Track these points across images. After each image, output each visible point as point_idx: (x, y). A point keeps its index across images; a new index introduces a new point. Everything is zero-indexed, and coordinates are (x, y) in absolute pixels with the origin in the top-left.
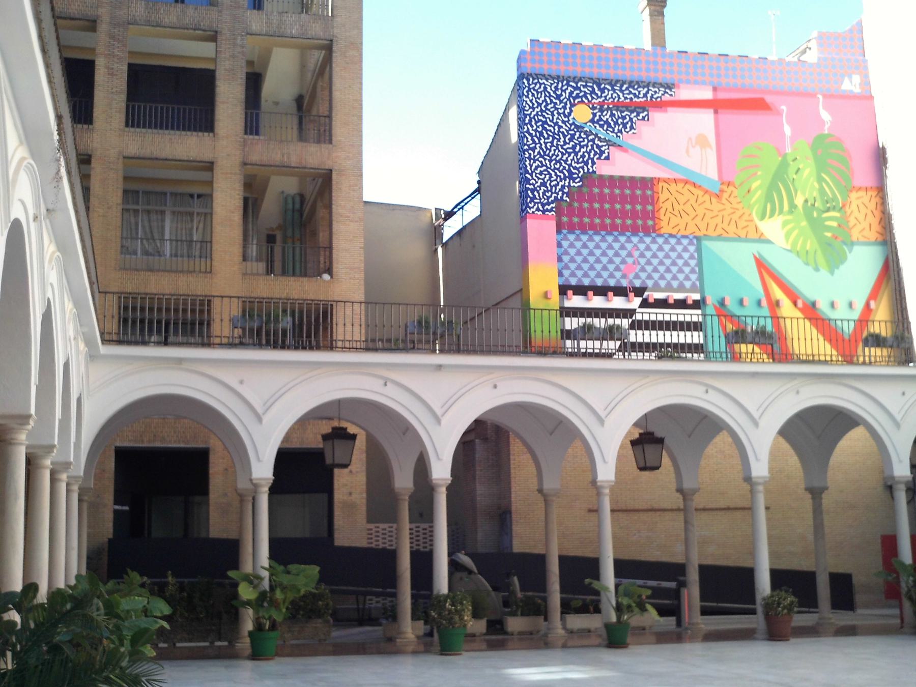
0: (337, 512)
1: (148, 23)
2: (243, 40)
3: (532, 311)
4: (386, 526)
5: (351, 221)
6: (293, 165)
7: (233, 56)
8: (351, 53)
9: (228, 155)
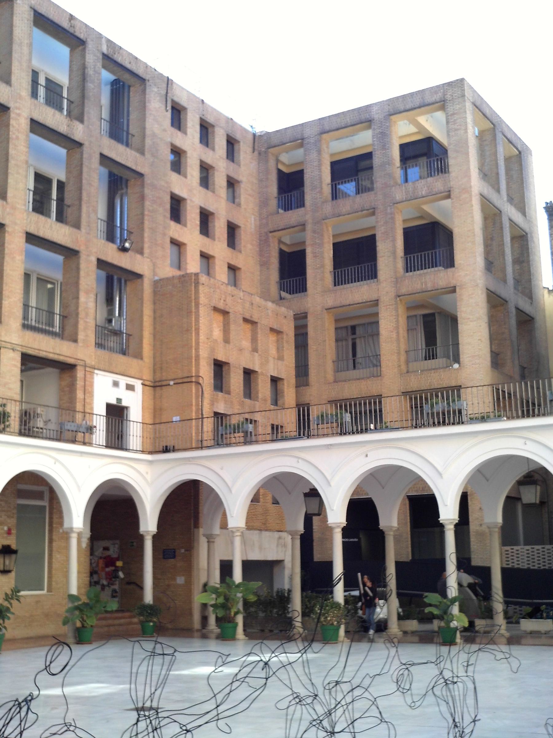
0: (473, 539)
2: (391, 209)
5: (471, 321)
6: (429, 289)
8: (464, 196)
9: (387, 293)
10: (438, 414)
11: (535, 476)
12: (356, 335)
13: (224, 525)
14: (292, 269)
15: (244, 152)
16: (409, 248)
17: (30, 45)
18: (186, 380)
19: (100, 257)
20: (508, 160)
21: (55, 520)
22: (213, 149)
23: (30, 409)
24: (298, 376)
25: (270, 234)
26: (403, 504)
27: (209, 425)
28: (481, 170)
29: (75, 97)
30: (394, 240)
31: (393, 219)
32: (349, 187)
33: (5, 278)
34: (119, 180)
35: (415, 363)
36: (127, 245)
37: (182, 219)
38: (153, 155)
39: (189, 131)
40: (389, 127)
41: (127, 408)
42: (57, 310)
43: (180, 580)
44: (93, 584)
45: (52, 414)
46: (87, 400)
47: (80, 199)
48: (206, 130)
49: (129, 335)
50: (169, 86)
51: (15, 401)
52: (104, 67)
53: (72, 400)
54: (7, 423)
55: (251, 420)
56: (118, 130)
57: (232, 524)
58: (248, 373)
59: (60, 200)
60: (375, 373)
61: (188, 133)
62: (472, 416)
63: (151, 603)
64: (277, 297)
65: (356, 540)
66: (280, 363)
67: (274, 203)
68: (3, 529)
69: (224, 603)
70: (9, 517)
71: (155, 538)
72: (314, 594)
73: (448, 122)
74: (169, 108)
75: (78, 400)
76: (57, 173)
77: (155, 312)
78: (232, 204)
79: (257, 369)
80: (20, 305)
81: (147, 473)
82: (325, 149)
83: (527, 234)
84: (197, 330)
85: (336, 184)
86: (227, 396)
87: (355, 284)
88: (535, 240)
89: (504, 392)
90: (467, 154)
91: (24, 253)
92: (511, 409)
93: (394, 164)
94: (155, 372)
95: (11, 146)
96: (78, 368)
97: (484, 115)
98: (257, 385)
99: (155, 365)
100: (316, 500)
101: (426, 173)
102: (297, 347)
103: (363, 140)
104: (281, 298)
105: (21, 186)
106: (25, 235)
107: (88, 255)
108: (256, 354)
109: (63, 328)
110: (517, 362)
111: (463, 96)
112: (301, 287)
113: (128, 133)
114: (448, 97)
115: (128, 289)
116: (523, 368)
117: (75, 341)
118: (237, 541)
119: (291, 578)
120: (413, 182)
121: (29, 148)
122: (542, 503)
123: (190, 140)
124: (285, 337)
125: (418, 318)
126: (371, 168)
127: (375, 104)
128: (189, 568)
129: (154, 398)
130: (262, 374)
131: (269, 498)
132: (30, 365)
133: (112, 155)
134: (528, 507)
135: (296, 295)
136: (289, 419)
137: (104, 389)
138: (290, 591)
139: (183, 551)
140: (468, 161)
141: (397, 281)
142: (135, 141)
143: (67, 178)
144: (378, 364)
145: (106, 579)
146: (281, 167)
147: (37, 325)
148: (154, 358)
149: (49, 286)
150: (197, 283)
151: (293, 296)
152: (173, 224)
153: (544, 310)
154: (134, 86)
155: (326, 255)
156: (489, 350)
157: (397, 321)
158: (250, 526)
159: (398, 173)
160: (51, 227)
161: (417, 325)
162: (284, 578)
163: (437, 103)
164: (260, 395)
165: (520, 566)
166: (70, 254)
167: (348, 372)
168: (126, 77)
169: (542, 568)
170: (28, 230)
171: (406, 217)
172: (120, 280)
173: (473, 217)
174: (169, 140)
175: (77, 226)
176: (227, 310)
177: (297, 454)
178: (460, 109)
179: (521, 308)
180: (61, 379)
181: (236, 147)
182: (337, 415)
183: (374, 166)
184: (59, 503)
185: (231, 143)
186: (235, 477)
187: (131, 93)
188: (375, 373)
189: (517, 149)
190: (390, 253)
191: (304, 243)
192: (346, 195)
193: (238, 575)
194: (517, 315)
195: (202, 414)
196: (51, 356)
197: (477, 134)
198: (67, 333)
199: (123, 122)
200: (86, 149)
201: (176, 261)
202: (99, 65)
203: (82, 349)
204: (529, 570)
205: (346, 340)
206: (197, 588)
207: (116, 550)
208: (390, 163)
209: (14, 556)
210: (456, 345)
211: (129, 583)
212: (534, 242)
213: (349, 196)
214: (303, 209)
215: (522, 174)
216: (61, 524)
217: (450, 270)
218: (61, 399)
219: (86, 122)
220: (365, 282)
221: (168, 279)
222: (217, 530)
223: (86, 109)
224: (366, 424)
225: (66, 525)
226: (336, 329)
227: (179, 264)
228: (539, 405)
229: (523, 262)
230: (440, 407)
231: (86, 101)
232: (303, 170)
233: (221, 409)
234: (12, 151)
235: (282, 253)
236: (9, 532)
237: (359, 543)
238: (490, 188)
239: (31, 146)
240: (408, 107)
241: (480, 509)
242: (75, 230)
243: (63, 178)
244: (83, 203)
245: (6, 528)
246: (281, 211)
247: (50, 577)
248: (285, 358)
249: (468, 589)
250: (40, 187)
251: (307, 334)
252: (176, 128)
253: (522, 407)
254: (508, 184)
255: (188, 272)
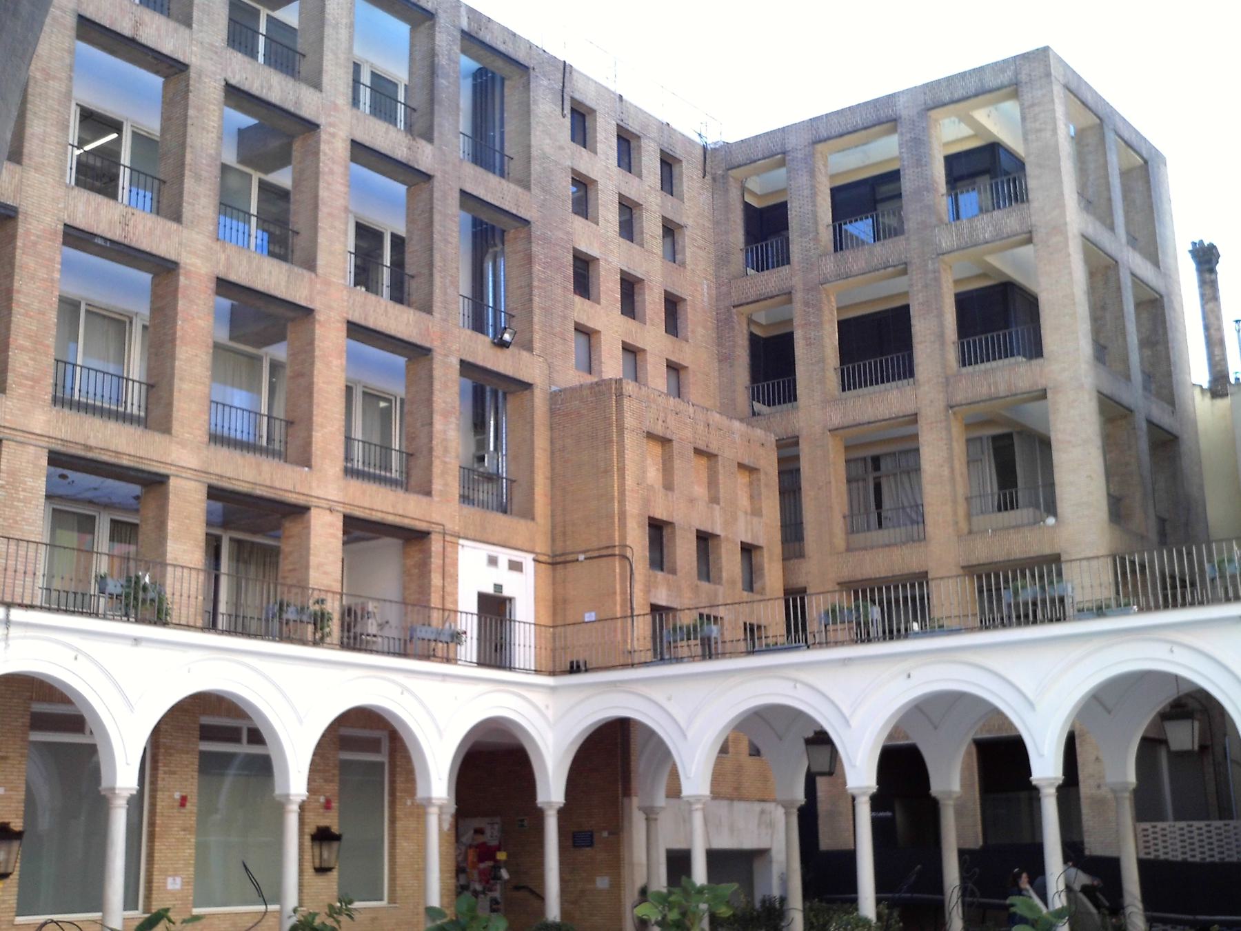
0: (1086, 810)
1: (839, 277)
3: (170, 569)
4: (1202, 824)
7: (926, 286)
10: (1026, 604)
11: (1194, 706)
12: (881, 470)
13: (675, 791)
14: (772, 365)
15: (690, 177)
16: (966, 327)
17: (351, 26)
18: (604, 552)
19: (464, 358)
20: (1125, 174)
21: (400, 785)
22: (640, 176)
23: (356, 604)
24: (785, 541)
25: (734, 310)
26: (968, 753)
27: (642, 627)
28: (1082, 194)
29: (419, 101)
30: (940, 315)
31: (937, 280)
32: (861, 228)
33: (315, 395)
34: (490, 231)
35: (981, 517)
36: (507, 337)
37: (593, 291)
38: (544, 190)
39: (600, 147)
40: (925, 130)
41: (510, 599)
42: (396, 444)
43: (602, 883)
44: (461, 889)
45: (392, 613)
46: (448, 589)
47: (431, 265)
48: (627, 142)
49: (511, 482)
50: (567, 75)
51: (334, 593)
52: (464, 51)
53: (425, 589)
54: (327, 630)
55: (716, 618)
56: (486, 149)
57: (688, 789)
58: (704, 539)
59: (398, 264)
60: (916, 535)
61: (599, 150)
62: (1081, 606)
63: (558, 920)
64: (748, 411)
65: (889, 814)
66: (755, 520)
67: (738, 258)
68: (318, 801)
69: (678, 921)
70: (326, 781)
71: (563, 813)
72: (824, 904)
73: (1024, 119)
74: (567, 111)
75: (433, 589)
76: (392, 223)
77: (552, 443)
78: (671, 264)
79: (718, 531)
80: (341, 438)
81: (547, 707)
82: (822, 167)
83: (1161, 296)
84: (622, 470)
85: (840, 226)
86: (670, 576)
87: (876, 388)
88: (1176, 306)
89: (1133, 563)
90: (1058, 170)
91: (345, 355)
92: (1145, 594)
93: (936, 190)
94: (553, 540)
95: (322, 185)
96: (433, 536)
97: (1083, 103)
98: (719, 558)
99: (553, 527)
100: (824, 751)
101: (990, 203)
102: (782, 492)
103: (882, 151)
104: (754, 414)
105: (338, 247)
106: (345, 326)
107: (446, 356)
108: (717, 507)
109: (407, 473)
110: (1151, 511)
111: (1048, 75)
112: (788, 394)
113: (503, 155)
114: (1023, 77)
115: (508, 406)
116: (1162, 521)
117: (428, 493)
118: (698, 819)
119: (784, 875)
120: (970, 219)
121: (349, 186)
122: (1203, 748)
123: (601, 163)
124: (762, 477)
125: (985, 442)
126: (898, 196)
127: (903, 92)
128: (616, 863)
129: (554, 583)
130: (727, 539)
131: (744, 747)
132: (357, 533)
133: (480, 192)
134: (1178, 757)
135: (778, 407)
136: (773, 616)
137: (475, 569)
138: (783, 900)
139: (605, 834)
140: (1061, 182)
141: (948, 382)
142: (513, 167)
143: (408, 231)
144: (920, 519)
145: (480, 881)
146: (748, 199)
147: (366, 469)
148: (553, 516)
149: (382, 404)
150: (620, 395)
151: (773, 409)
152: (577, 299)
153: (1195, 423)
154: (510, 78)
155: (827, 341)
156: (1105, 493)
157: (950, 449)
158: (716, 795)
159: (943, 203)
160: (386, 311)
161: (983, 452)
162: (770, 878)
163: (1005, 87)
164: (724, 575)
165: (1170, 857)
166: (417, 353)
167: (868, 534)
168: (498, 65)
169: (1208, 860)
170: (350, 319)
171: (958, 277)
172: (495, 393)
173: (1070, 274)
174: (569, 163)
175: (427, 309)
176: (668, 436)
177: (794, 674)
178: (1044, 96)
179: (1155, 421)
180: (405, 555)
181: (676, 170)
182: (857, 608)
183: (903, 194)
184: (408, 759)
185: (668, 163)
186: (691, 713)
187: (506, 90)
188: (916, 535)
189: (1142, 157)
190: (934, 334)
191: (791, 321)
192: (859, 243)
193: (700, 873)
194: (1150, 432)
195: (632, 608)
196: (390, 519)
197: (1072, 133)
198: (413, 482)
199: (494, 137)
200: (437, 183)
201: (586, 360)
202: (456, 49)
203: (439, 508)
204: (1185, 863)
205: (864, 480)
206: (630, 895)
207: (496, 833)
208: (930, 188)
209: (335, 845)
210: (1050, 485)
211: (517, 888)
212: (1174, 310)
213: (863, 242)
214: (787, 267)
215: (1150, 197)
216: (412, 791)
217: (1036, 363)
218: (405, 588)
219: (436, 141)
220: (894, 384)
221: (573, 389)
222: (661, 800)
223: (437, 120)
224: (907, 622)
225: (420, 794)
226: (847, 461)
227: (589, 363)
228: (1193, 584)
229: (1156, 343)
230: (1029, 592)
231: (436, 107)
232: (785, 204)
233: (662, 599)
234: (323, 193)
235: (753, 339)
236: (327, 806)
237: (893, 819)
238: (1098, 224)
239: (354, 185)
240: (956, 96)
241: (1097, 759)
242: (424, 315)
243: (402, 231)
244: (435, 271)
245: (322, 799)
246: (751, 271)
247: (393, 879)
248: (764, 512)
249: (1081, 895)
250: (364, 245)
251: (798, 470)
252: (578, 143)
253: (1164, 588)
254: (1127, 213)
255: (606, 376)
